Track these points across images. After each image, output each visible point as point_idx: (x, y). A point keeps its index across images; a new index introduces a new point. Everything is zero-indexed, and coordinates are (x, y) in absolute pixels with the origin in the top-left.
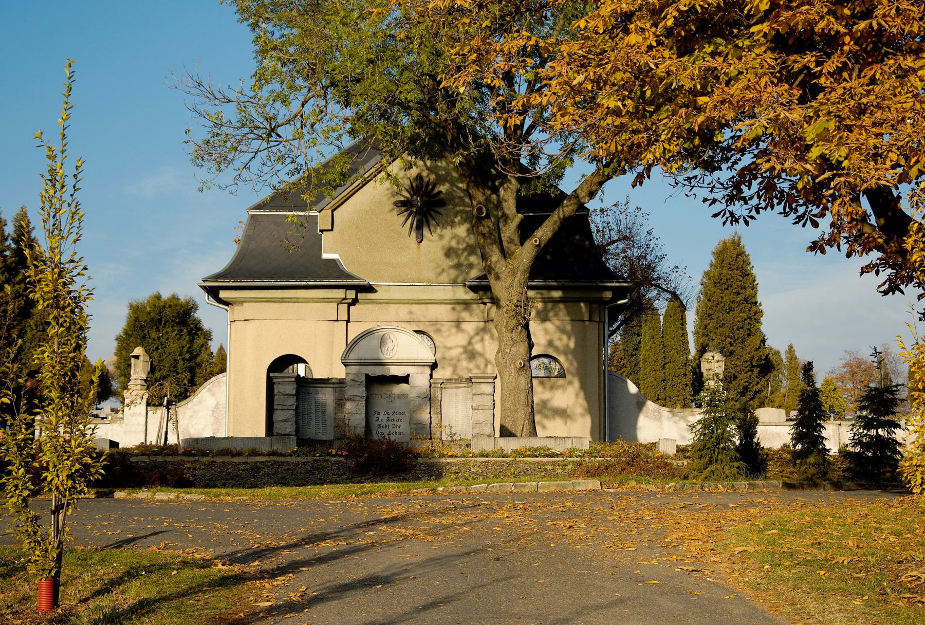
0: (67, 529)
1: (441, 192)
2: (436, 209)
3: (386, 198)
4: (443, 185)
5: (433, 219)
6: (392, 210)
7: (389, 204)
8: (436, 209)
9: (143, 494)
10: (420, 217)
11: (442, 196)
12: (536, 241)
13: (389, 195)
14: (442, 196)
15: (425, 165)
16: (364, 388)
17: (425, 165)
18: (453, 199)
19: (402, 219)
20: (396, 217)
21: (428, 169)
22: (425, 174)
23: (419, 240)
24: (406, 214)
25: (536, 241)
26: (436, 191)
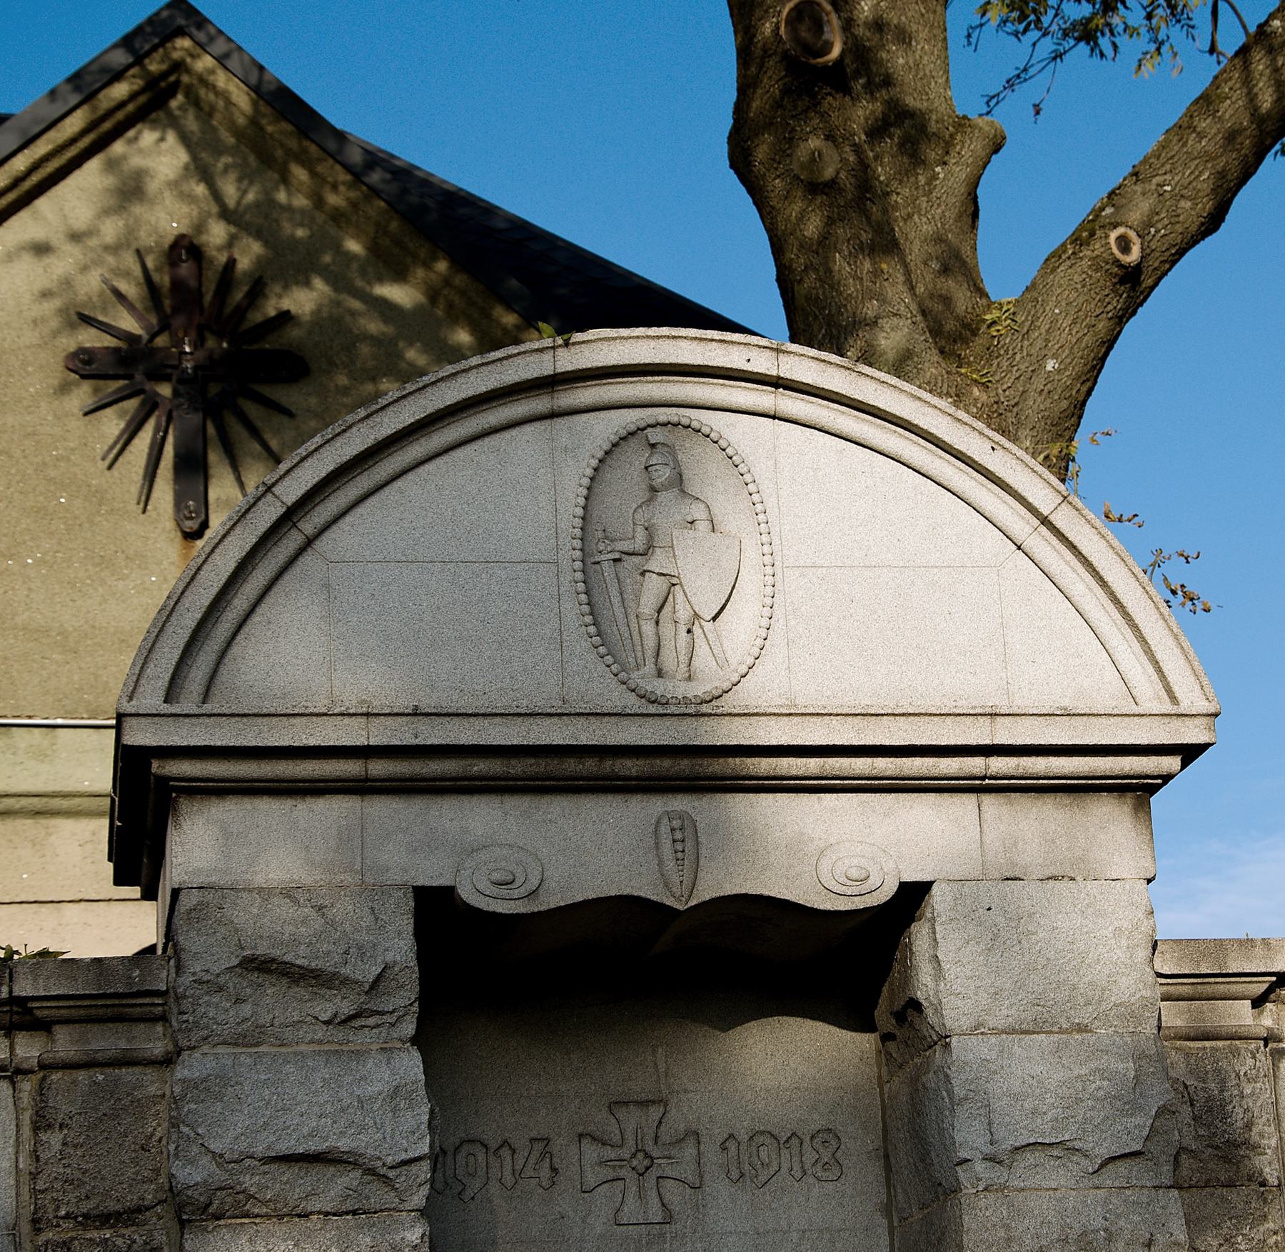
0: (666, 1153)
1: (285, 317)
2: (266, 390)
3: (30, 337)
4: (307, 284)
5: (255, 433)
6: (64, 389)
7: (50, 365)
8: (266, 390)
9: (129, 391)
10: (195, 418)
11: (295, 333)
12: (1124, 244)
13: (55, 323)
14: (295, 333)
15: (216, 195)
16: (411, 1065)
17: (216, 195)
18: (351, 340)
19: (112, 423)
20: (77, 424)
21: (226, 214)
22: (217, 233)
23: (191, 525)
24: (132, 404)
25: (1124, 244)
26: (270, 309)
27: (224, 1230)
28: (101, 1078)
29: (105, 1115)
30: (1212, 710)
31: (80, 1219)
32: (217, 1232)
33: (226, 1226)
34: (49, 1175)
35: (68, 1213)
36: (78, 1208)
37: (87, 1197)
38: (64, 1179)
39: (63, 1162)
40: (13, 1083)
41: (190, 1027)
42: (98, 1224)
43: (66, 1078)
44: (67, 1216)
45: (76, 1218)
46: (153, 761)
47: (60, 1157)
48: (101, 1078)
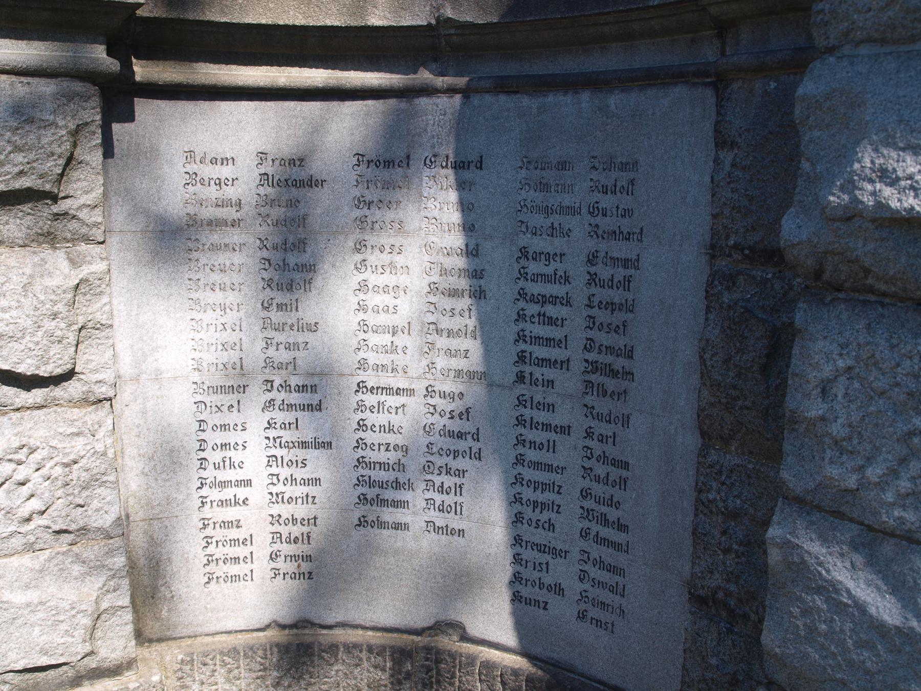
27: (843, 306)
28: (773, 85)
29: (771, 133)
30: (244, 368)
31: (747, 252)
32: (834, 307)
33: (845, 300)
34: (720, 200)
35: (735, 243)
36: (746, 239)
37: (753, 229)
38: (732, 205)
39: (732, 185)
40: (716, 90)
41: (826, 18)
42: (763, 260)
43: (745, 86)
44: (736, 246)
45: (742, 250)
46: (134, 60)
47: (728, 180)
48: (773, 85)
